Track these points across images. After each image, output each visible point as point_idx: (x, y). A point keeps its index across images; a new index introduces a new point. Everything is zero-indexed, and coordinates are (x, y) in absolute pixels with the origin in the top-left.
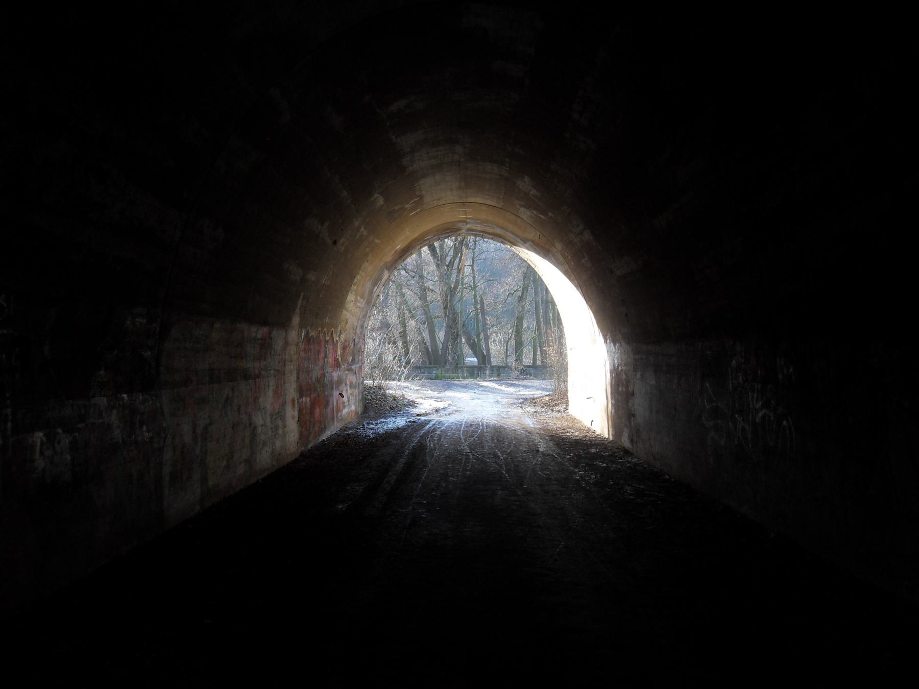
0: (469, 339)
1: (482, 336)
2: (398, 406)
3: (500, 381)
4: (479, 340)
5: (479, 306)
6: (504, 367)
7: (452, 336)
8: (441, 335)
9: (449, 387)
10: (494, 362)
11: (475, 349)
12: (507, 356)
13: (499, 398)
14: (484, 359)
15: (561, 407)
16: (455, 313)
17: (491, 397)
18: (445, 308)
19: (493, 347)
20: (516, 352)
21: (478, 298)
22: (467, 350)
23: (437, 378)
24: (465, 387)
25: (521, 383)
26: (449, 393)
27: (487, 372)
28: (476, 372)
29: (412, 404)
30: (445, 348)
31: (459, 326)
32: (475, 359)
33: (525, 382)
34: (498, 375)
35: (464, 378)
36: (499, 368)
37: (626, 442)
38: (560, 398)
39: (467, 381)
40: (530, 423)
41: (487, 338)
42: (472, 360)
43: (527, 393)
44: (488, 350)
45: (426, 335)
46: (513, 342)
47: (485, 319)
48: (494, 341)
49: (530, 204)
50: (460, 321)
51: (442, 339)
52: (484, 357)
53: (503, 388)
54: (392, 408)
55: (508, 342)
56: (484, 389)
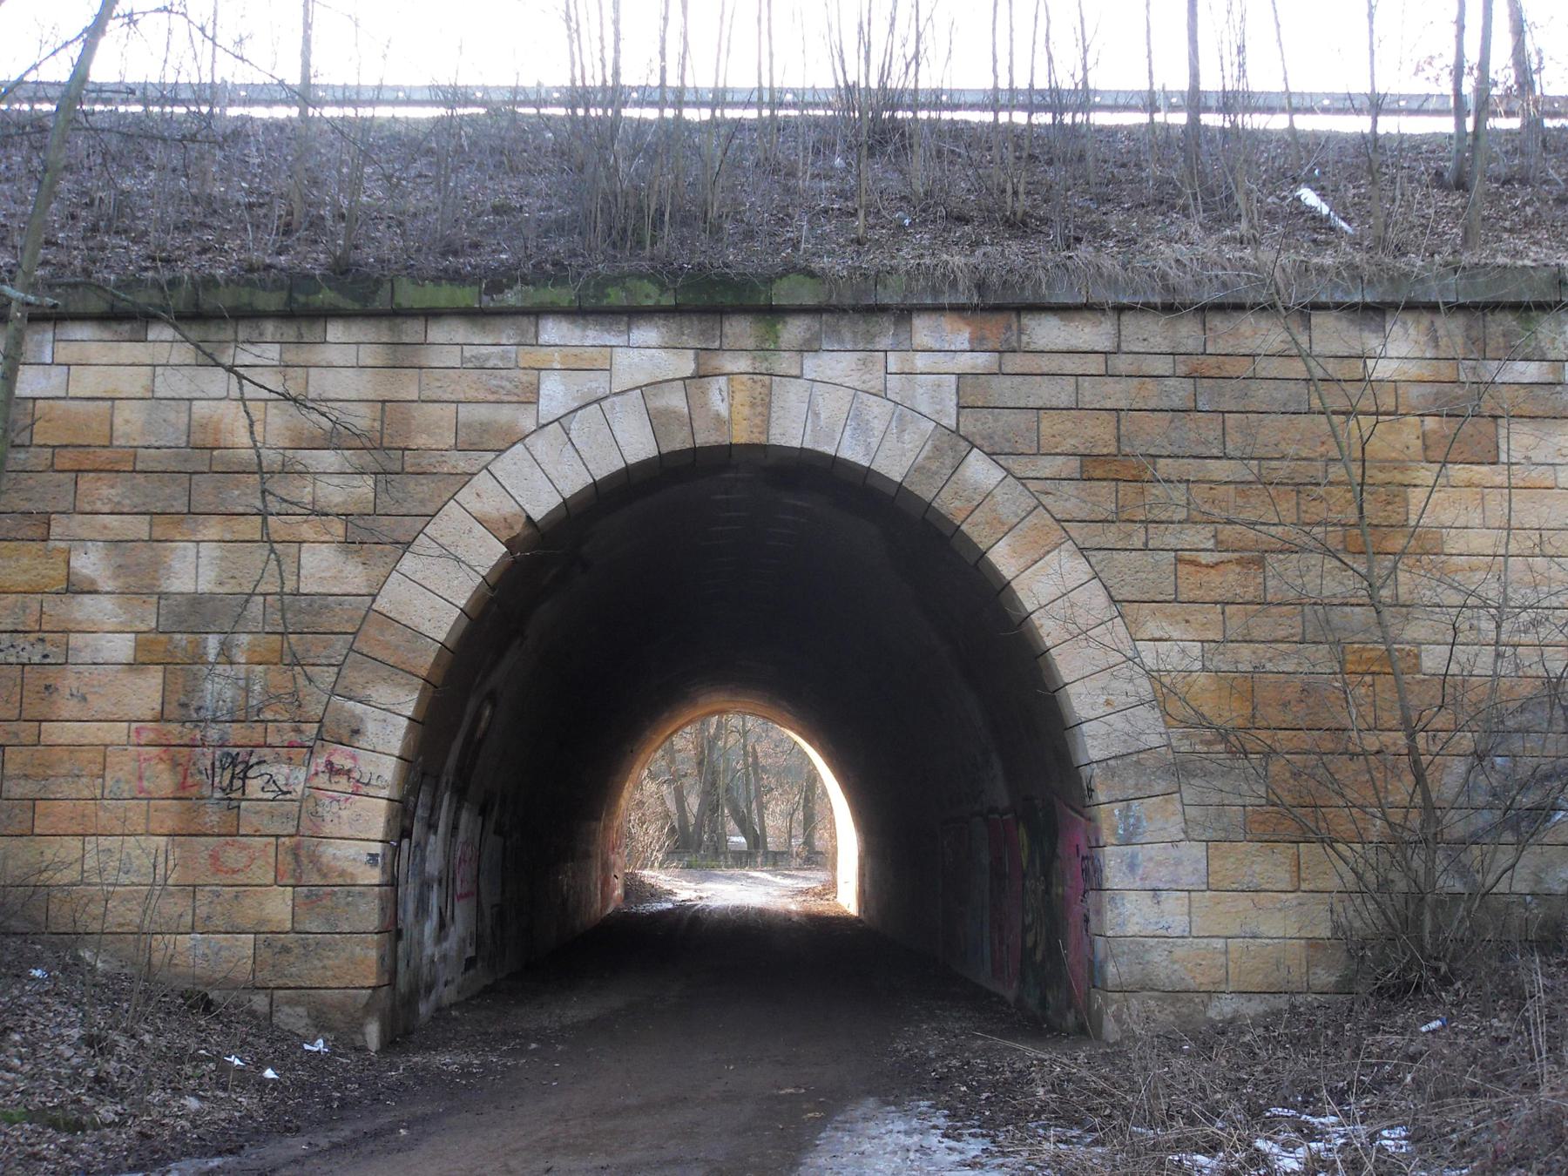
0: (735, 812)
1: (754, 806)
2: (656, 894)
3: (774, 872)
4: (750, 811)
5: (750, 760)
6: (783, 853)
7: (711, 807)
8: (693, 803)
9: (708, 878)
10: (772, 844)
11: (745, 826)
12: (790, 837)
13: (771, 890)
14: (757, 840)
15: (830, 897)
16: (714, 773)
17: (761, 889)
18: (700, 763)
19: (769, 822)
20: (805, 830)
21: (749, 748)
22: (732, 825)
23: (689, 866)
24: (730, 878)
25: (801, 873)
26: (707, 885)
27: (759, 860)
28: (743, 859)
29: (670, 893)
30: (699, 825)
31: (721, 791)
32: (743, 840)
33: (807, 873)
34: (775, 864)
35: (727, 867)
36: (776, 853)
37: (862, 917)
38: (831, 887)
39: (731, 872)
40: (794, 906)
41: (762, 807)
42: (738, 841)
43: (804, 885)
44: (763, 829)
45: (671, 806)
46: (800, 815)
47: (760, 779)
48: (773, 811)
49: (788, 712)
50: (722, 782)
51: (695, 810)
52: (756, 837)
53: (778, 879)
54: (652, 895)
55: (792, 815)
56: (466, 263)
